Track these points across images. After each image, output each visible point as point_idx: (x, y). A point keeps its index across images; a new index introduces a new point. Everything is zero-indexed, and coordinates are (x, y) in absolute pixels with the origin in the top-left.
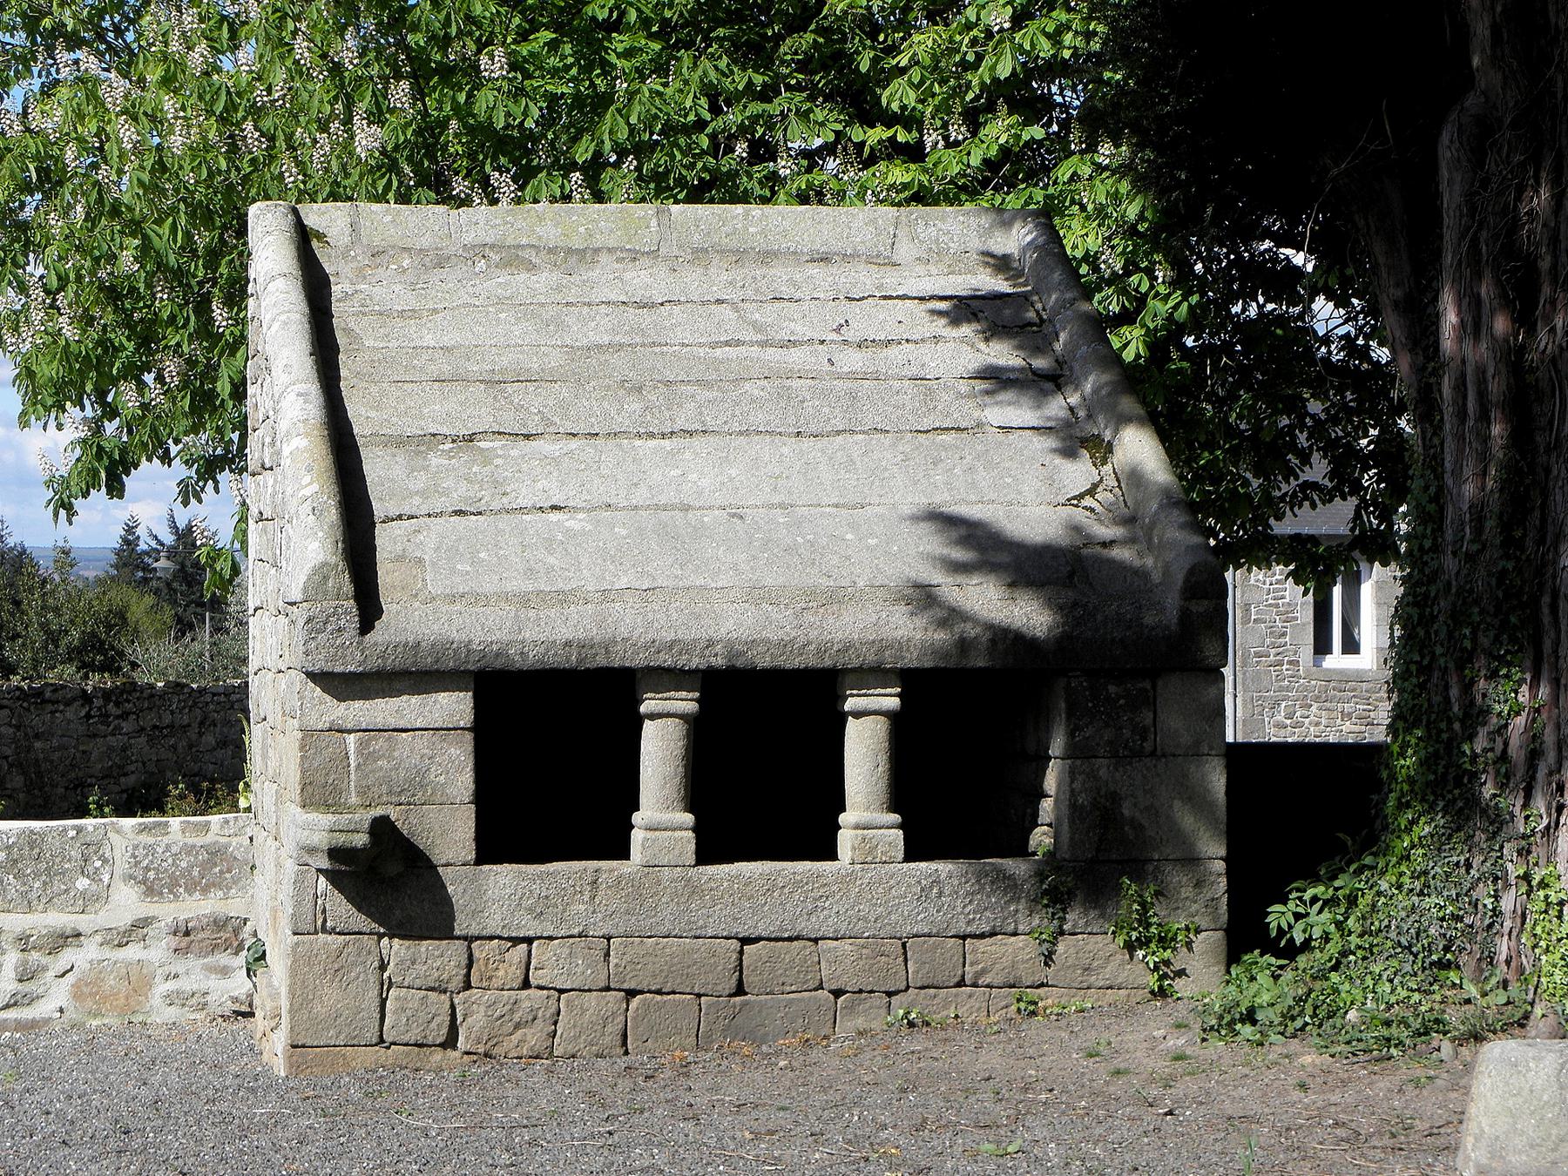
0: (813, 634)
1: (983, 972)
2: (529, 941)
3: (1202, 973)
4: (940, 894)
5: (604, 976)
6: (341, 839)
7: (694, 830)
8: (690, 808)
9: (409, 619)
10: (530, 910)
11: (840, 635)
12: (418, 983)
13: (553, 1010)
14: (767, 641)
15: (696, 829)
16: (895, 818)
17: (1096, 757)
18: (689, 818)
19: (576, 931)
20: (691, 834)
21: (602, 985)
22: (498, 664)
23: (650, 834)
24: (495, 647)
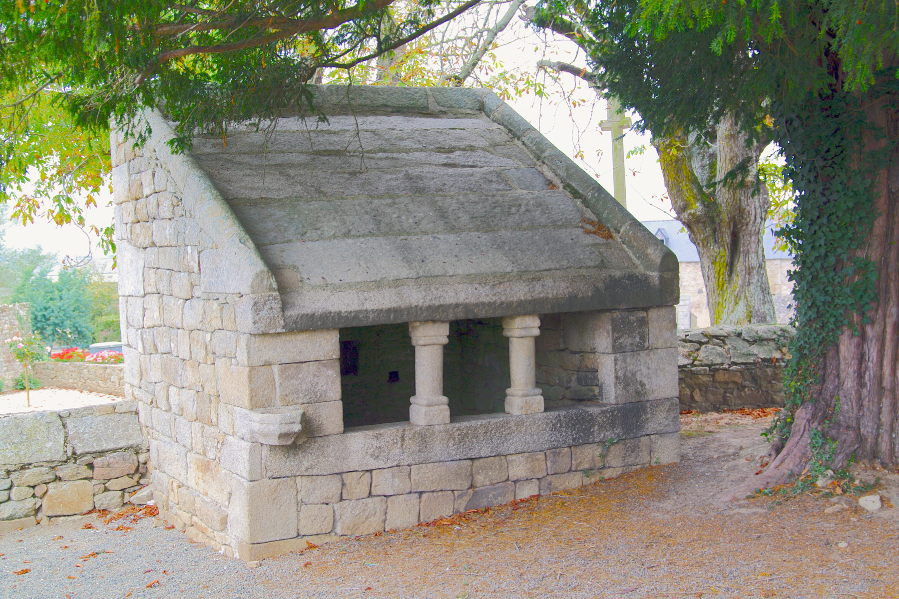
0: (503, 298)
1: (581, 463)
2: (371, 471)
3: (727, 133)
4: (561, 427)
5: (409, 486)
6: (285, 429)
7: (449, 405)
8: (445, 394)
9: (312, 302)
10: (372, 455)
11: (515, 299)
12: (317, 501)
13: (385, 507)
14: (483, 304)
15: (450, 405)
16: (539, 391)
17: (403, 42)
18: (445, 399)
19: (395, 464)
20: (447, 407)
21: (408, 491)
22: (354, 324)
23: (428, 409)
24: (353, 314)
